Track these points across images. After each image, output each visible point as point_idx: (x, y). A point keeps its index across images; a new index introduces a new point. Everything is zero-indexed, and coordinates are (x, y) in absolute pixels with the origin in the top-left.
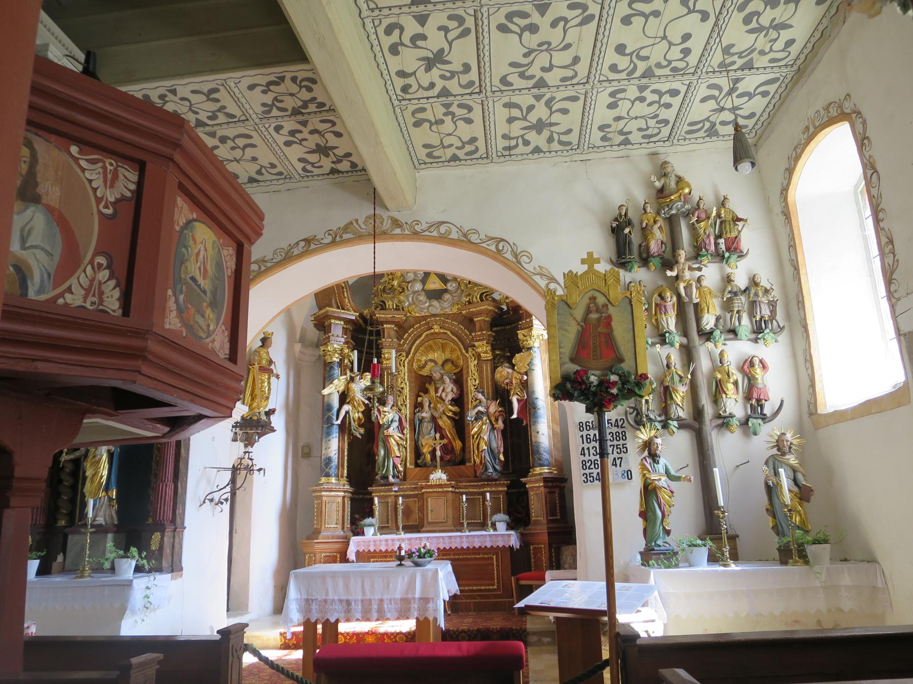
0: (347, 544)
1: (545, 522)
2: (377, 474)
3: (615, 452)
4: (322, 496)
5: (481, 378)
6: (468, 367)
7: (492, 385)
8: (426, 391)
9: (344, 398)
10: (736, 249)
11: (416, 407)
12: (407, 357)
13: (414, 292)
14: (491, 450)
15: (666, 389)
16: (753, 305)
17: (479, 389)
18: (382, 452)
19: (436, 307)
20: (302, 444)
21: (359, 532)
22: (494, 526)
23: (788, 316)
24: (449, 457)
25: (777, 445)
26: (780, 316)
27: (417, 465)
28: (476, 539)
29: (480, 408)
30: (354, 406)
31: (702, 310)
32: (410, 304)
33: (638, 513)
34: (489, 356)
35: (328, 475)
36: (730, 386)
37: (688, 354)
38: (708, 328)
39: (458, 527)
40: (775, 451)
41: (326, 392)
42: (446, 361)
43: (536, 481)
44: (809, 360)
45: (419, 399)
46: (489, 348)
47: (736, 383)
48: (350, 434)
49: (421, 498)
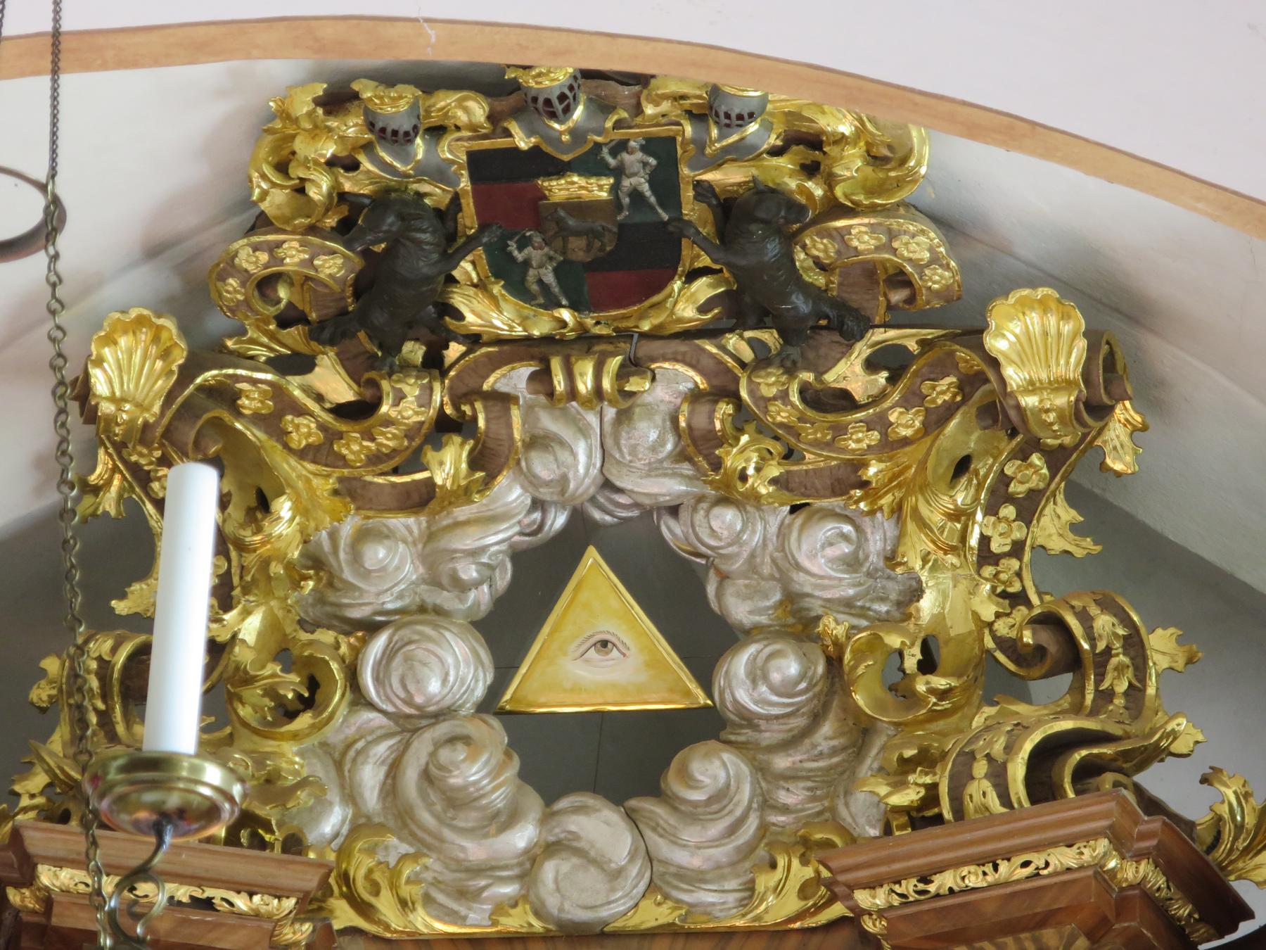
13: (412, 722)
32: (360, 826)
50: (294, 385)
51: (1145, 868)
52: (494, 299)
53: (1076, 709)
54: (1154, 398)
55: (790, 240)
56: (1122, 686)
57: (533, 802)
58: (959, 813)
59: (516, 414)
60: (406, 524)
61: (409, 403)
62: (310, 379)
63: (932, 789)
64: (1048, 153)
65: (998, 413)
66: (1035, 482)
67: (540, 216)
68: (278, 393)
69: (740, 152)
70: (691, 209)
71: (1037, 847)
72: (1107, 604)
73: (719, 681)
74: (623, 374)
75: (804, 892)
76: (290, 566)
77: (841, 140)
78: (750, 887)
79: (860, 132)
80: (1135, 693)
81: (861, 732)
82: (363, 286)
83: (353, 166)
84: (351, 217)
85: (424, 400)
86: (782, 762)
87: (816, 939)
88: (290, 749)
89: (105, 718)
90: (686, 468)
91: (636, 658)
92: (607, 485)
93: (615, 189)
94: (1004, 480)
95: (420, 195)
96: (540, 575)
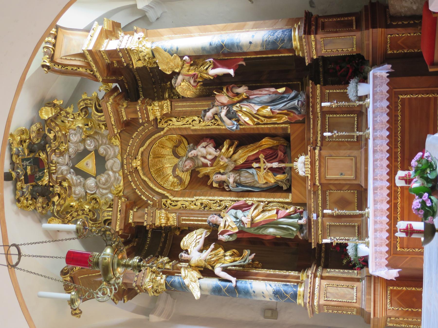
0: (377, 279)
1: (359, 34)
2: (297, 236)
4: (319, 305)
5: (191, 114)
6: (180, 129)
7: (199, 101)
8: (207, 177)
9: (207, 272)
11: (224, 190)
12: (167, 197)
13: (97, 187)
14: (273, 102)
17: (202, 115)
18: (271, 231)
19: (114, 163)
20: (262, 318)
21: (364, 262)
22: (361, 98)
24: (280, 153)
27: (289, 190)
28: (378, 119)
29: (223, 114)
30: (217, 261)
32: (110, 192)
34: (166, 104)
35: (295, 296)
39: (361, 143)
41: (197, 294)
42: (176, 155)
43: (309, 43)
45: (215, 185)
46: (156, 103)
48: (252, 265)
49: (326, 187)
50: (56, 203)
51: (110, 99)
52: (44, 180)
53: (92, 107)
54: (53, 98)
55: (34, 144)
56: (89, 101)
57: (107, 172)
58: (105, 121)
59: (59, 176)
60: (73, 189)
61: (58, 189)
62: (55, 202)
63: (102, 124)
64: (12, 117)
65: (56, 117)
66: (64, 112)
67: (32, 175)
68: (57, 205)
69: (23, 150)
70: (31, 156)
71: (108, 112)
72: (79, 103)
73: (91, 150)
74: (53, 164)
75: (116, 139)
76: (79, 203)
77: (21, 138)
78: (116, 146)
79: (20, 136)
80: (90, 100)
81: (96, 133)
82: (43, 196)
83: (27, 198)
84: (34, 198)
85: (57, 187)
86: (100, 142)
87: (122, 138)
88: (101, 201)
89: (99, 224)
90: (64, 155)
91: (88, 160)
92: (67, 165)
93: (29, 166)
94: (64, 116)
95: (31, 190)
96: (79, 172)
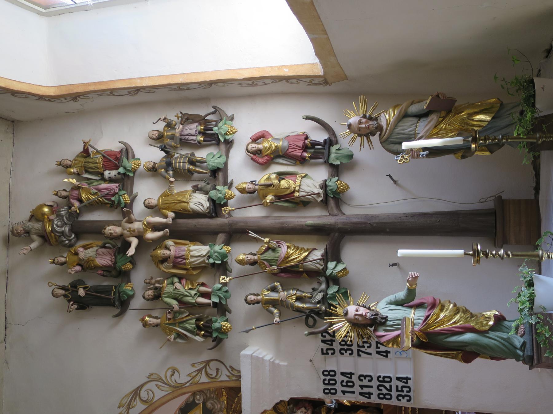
3: (368, 350)
10: (117, 159)
15: (284, 271)
16: (184, 143)
23: (202, 100)
25: (367, 136)
26: (202, 111)
31: (184, 210)
33: (464, 364)
36: (284, 183)
37: (237, 233)
38: (207, 204)
40: (375, 139)
44: (253, 81)
47: (281, 176)
